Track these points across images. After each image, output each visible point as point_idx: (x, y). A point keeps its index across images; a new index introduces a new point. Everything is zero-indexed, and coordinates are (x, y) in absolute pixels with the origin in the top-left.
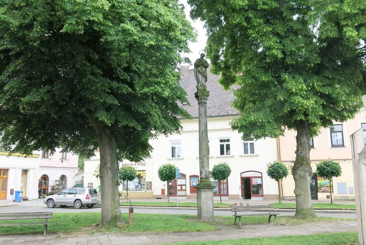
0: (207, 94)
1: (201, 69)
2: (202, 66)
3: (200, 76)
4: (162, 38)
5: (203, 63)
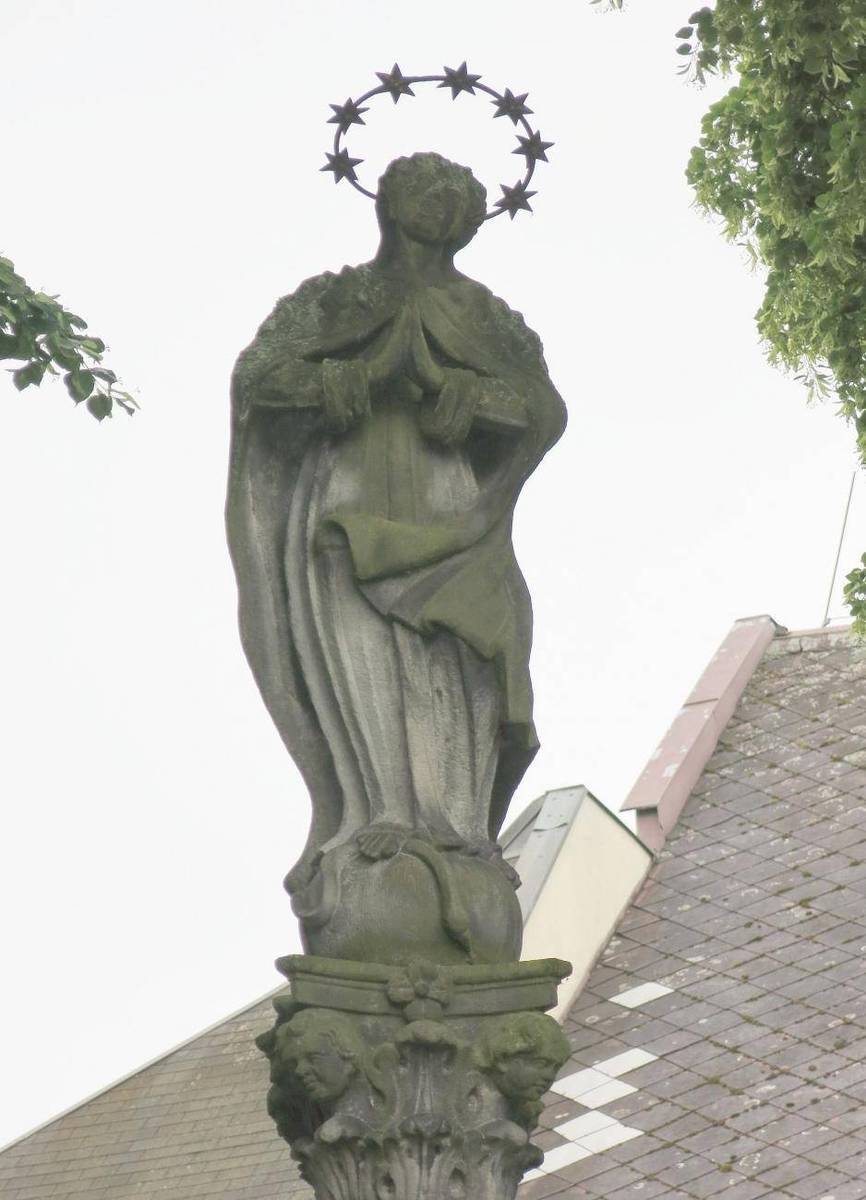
0: (506, 1035)
1: (386, 494)
2: (395, 440)
3: (358, 647)
4: (427, 162)
5: (407, 368)
